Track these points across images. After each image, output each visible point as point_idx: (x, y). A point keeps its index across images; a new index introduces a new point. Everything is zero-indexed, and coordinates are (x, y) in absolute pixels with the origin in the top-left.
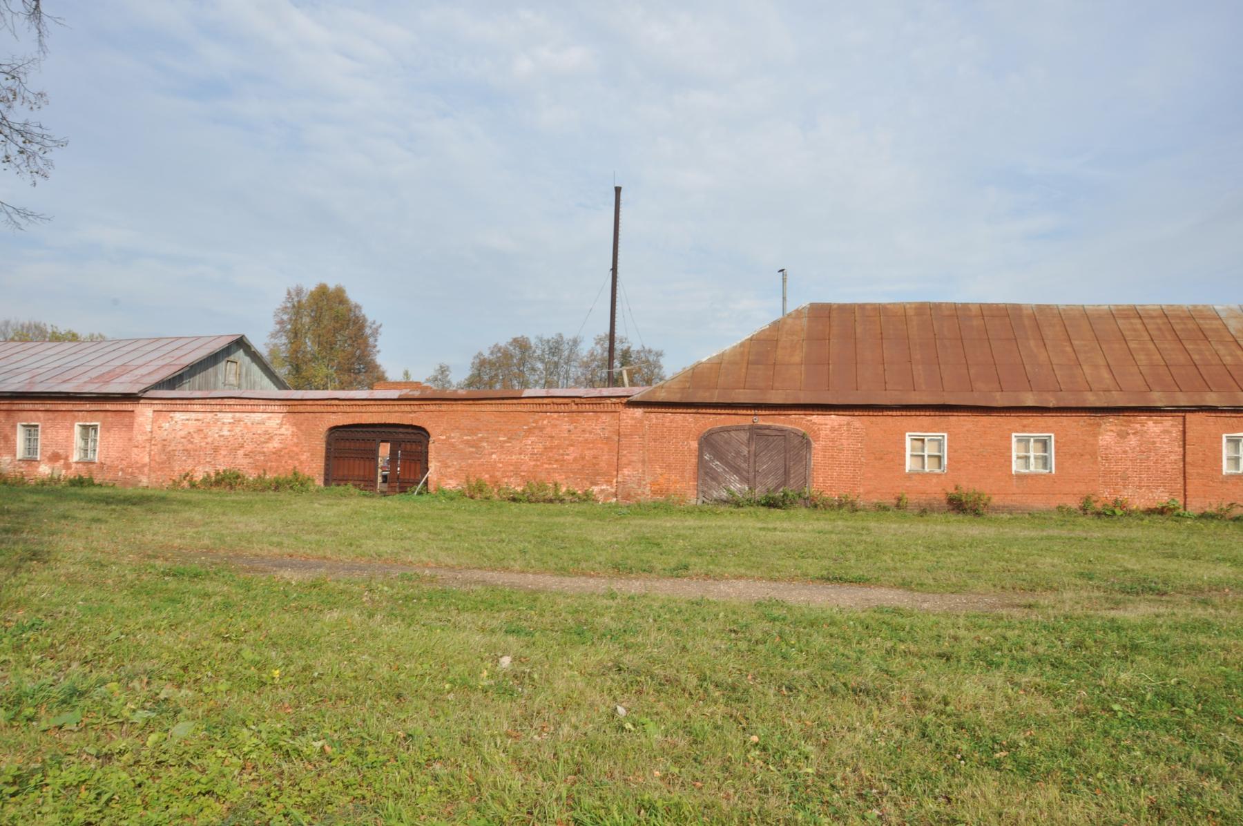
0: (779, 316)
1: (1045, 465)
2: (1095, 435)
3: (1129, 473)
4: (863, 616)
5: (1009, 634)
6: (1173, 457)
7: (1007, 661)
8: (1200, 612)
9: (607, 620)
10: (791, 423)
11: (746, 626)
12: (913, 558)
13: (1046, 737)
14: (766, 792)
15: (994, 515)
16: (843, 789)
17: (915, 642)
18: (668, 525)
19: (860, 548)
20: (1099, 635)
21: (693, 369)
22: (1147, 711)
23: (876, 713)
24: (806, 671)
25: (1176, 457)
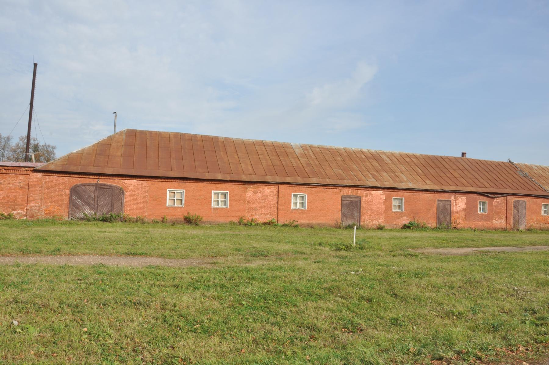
0: (112, 134)
1: (225, 205)
2: (245, 192)
3: (258, 208)
4: (141, 270)
5: (204, 275)
6: (274, 202)
7: (202, 287)
8: (279, 263)
9: (13, 277)
10: (115, 183)
11: (86, 277)
12: (167, 244)
13: (216, 317)
14: (89, 354)
15: (203, 225)
16: (126, 348)
17: (164, 280)
18: (52, 230)
19: (144, 240)
20: (240, 274)
21: (69, 155)
22: (255, 303)
23: (143, 313)
24: (112, 296)
25: (275, 202)
